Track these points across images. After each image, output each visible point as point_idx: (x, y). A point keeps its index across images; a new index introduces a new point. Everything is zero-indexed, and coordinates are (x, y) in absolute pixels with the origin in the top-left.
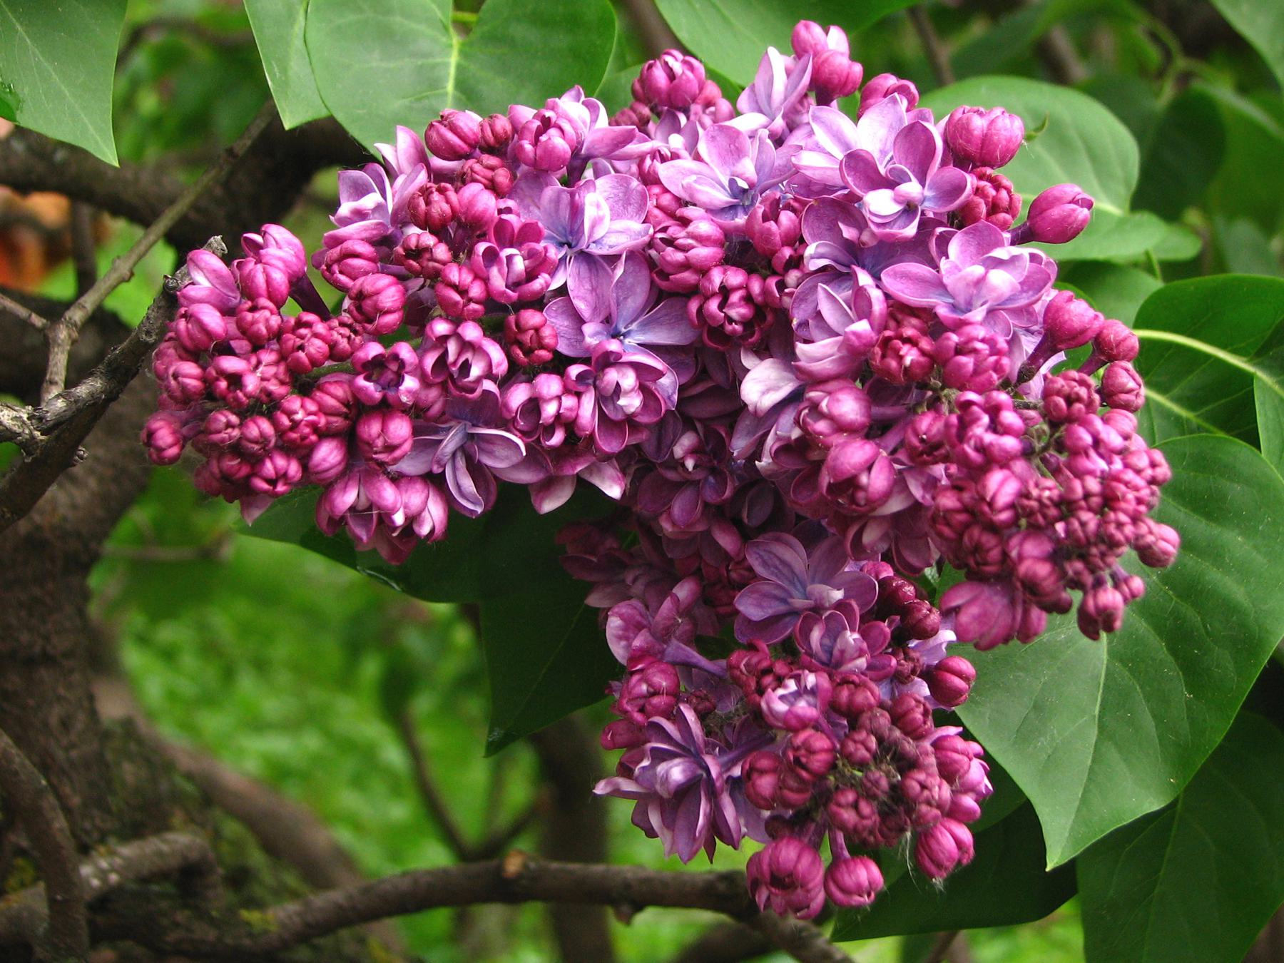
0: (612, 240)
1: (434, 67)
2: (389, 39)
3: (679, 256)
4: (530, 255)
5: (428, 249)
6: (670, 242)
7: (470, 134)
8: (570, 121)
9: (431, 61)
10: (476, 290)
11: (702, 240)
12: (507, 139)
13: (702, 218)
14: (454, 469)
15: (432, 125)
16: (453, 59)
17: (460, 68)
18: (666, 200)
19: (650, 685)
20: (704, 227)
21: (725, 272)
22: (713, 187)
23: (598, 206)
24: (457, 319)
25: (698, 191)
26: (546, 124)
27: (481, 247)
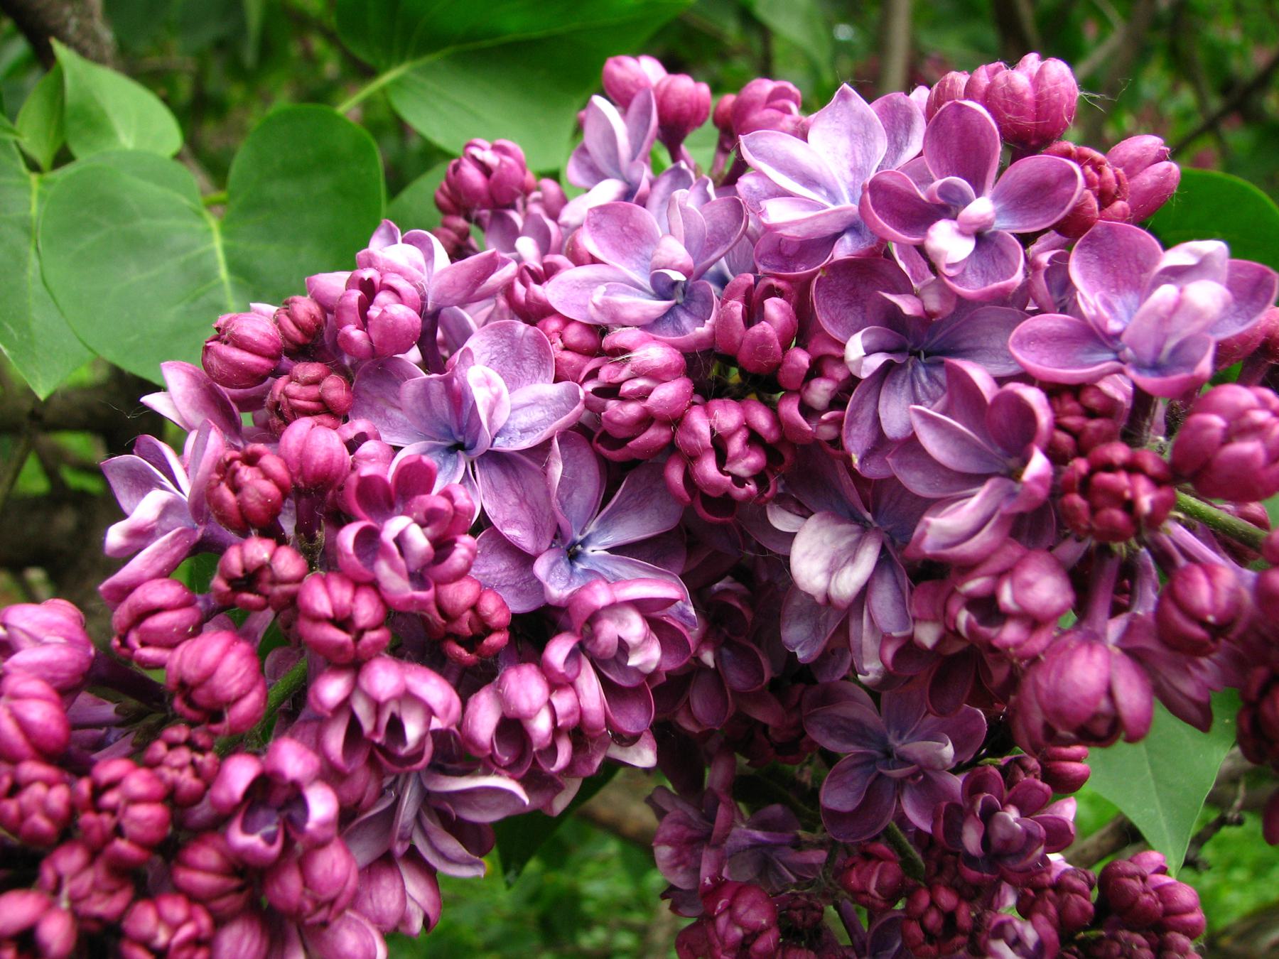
0: (523, 419)
1: (200, 258)
2: (140, 246)
3: (632, 409)
4: (429, 518)
5: (264, 567)
6: (611, 391)
7: (266, 342)
8: (400, 273)
9: (194, 253)
10: (366, 609)
11: (657, 375)
12: (319, 326)
13: (643, 342)
14: (426, 834)
15: (207, 349)
16: (217, 243)
17: (228, 251)
18: (573, 334)
19: (742, 925)
20: (654, 354)
21: (709, 414)
22: (627, 292)
23: (489, 382)
24: (354, 665)
25: (621, 306)
26: (369, 290)
27: (348, 536)
